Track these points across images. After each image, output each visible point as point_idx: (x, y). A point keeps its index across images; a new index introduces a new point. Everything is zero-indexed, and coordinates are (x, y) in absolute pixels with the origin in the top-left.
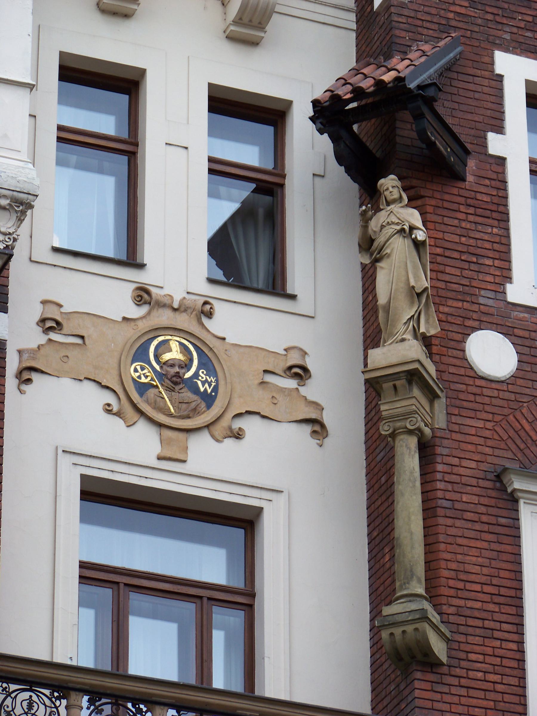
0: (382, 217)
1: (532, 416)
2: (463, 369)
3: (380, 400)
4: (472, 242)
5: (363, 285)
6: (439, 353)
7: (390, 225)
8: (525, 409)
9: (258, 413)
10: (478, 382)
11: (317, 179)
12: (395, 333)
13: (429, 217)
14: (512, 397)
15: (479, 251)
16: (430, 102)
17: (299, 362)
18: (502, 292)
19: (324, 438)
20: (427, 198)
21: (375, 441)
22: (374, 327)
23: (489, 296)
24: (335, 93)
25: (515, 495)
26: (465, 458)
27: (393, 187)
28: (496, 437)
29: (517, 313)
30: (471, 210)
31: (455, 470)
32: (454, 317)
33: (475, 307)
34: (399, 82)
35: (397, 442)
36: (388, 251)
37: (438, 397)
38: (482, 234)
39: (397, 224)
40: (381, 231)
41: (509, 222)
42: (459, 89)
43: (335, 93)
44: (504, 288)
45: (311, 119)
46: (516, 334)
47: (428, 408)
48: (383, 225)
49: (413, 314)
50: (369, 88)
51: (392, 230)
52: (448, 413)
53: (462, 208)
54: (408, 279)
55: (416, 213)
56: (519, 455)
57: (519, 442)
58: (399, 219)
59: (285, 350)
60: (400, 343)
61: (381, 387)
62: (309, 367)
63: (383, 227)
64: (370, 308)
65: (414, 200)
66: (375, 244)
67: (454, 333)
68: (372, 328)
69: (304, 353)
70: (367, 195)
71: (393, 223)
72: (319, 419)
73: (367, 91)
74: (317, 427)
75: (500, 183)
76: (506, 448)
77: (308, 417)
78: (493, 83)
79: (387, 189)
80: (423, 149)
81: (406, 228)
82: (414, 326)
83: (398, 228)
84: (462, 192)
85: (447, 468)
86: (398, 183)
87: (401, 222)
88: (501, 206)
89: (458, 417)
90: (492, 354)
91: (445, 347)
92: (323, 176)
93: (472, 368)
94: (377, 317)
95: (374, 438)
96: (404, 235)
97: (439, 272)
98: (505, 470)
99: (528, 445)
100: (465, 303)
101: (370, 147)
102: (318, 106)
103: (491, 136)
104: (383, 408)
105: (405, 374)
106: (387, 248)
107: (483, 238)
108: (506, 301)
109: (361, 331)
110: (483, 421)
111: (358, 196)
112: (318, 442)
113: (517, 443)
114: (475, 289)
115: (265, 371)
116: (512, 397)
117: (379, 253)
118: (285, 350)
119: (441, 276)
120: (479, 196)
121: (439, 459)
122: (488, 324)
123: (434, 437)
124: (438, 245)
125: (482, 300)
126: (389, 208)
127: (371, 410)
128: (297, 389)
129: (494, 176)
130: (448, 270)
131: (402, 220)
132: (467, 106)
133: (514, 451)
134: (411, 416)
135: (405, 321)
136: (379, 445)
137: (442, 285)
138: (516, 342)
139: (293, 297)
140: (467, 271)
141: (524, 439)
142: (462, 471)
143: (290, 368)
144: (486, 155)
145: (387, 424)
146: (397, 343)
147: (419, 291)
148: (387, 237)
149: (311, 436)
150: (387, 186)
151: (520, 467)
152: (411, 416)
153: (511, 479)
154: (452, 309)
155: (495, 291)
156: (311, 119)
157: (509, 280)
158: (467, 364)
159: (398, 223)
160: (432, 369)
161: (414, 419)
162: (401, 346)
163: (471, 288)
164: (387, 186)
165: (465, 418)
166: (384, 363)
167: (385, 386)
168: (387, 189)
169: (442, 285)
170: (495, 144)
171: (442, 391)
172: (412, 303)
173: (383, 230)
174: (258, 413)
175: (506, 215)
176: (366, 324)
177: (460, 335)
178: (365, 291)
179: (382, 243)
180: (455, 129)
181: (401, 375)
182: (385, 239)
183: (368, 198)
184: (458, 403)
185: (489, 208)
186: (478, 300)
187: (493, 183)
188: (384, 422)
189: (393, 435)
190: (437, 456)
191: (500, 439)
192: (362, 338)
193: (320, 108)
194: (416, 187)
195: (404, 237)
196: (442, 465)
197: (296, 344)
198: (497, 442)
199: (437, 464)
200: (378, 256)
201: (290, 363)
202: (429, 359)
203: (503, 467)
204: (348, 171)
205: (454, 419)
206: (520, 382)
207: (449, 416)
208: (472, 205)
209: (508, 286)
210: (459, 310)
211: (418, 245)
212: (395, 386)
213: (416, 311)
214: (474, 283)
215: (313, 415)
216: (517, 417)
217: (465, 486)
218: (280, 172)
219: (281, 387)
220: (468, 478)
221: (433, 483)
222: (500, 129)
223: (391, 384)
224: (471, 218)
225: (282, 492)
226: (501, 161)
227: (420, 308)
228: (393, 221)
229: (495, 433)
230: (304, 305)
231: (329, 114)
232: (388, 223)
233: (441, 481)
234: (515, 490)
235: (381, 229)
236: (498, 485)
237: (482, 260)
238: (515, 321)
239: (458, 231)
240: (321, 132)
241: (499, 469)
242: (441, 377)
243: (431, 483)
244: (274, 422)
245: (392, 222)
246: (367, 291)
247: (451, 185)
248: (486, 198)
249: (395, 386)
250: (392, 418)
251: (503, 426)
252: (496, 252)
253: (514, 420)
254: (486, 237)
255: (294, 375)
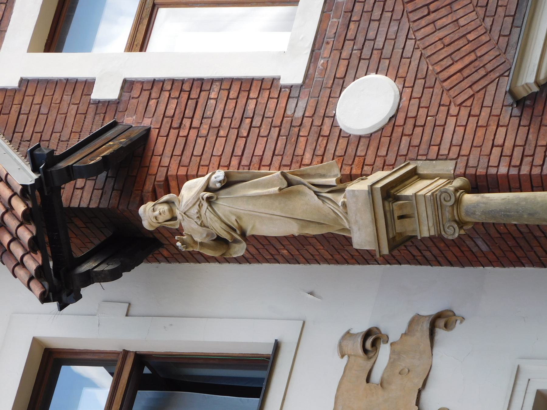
0: (190, 227)
1: (445, 60)
2: (382, 139)
3: (417, 236)
4: (226, 123)
5: (267, 261)
6: (361, 167)
7: (201, 215)
8: (436, 68)
9: (420, 392)
10: (400, 120)
11: (132, 311)
12: (334, 215)
13: (192, 171)
14: (420, 82)
15: (238, 115)
16: (52, 159)
17: (359, 340)
18: (290, 90)
19: (454, 315)
20: (169, 173)
21: (463, 252)
22: (322, 248)
23: (294, 105)
24: (34, 275)
25: (543, 83)
26: (493, 140)
27: (154, 210)
28: (468, 103)
29: (316, 73)
30: (187, 122)
31: (507, 152)
32: (318, 147)
33: (307, 122)
34: (28, 193)
35: (468, 219)
36: (233, 218)
37: (415, 169)
38: (217, 111)
39: (200, 206)
40: (208, 228)
41: (203, 79)
42: (35, 131)
43: (34, 275)
44: (286, 87)
45: (61, 307)
46: (343, 76)
47: (428, 182)
48: (201, 224)
49: (312, 192)
50: (31, 232)
51: (208, 213)
52: (437, 159)
53: (183, 133)
54: (269, 196)
55: (187, 184)
56: (493, 76)
57: (476, 76)
58: (194, 204)
59: (342, 356)
60: (348, 208)
61: (400, 234)
62: (364, 328)
63: (202, 225)
64: (297, 253)
65: (171, 185)
66: (224, 235)
67: (338, 148)
68: (323, 252)
69: (348, 334)
70: (157, 252)
71: (199, 212)
72: (430, 319)
73: (35, 233)
74: (442, 321)
75: (154, 87)
76: (483, 92)
77: (427, 333)
78: (30, 91)
79: (156, 218)
80: (107, 177)
81: (208, 194)
82: (328, 192)
83: (205, 204)
84: (164, 132)
85: (505, 161)
86: (150, 204)
87: (198, 201)
88: (183, 87)
89: (442, 147)
90: (368, 103)
91: (354, 159)
92: (130, 304)
93: (382, 129)
94: (314, 237)
95: (459, 254)
96: (215, 199)
97: (260, 163)
98: (511, 92)
99: (481, 65)
100: (301, 134)
101: (102, 240)
102: (48, 296)
103: (97, 95)
104: (426, 234)
105: (386, 203)
106: (230, 221)
107: (222, 109)
108: (302, 86)
109: (324, 267)
110: (448, 117)
111: (155, 265)
112: (458, 322)
113: (478, 78)
114: (284, 121)
115: (368, 380)
116: (420, 82)
117: (234, 230)
118: (342, 356)
119: (267, 160)
120: (170, 112)
121: (493, 171)
122: (328, 107)
123: (464, 175)
124: (228, 163)
125: (299, 114)
126: (179, 217)
127: (424, 256)
128: (391, 344)
129: (146, 94)
130: (259, 152)
131: (196, 200)
132: (56, 122)
133: (487, 83)
134: (438, 199)
135: (320, 202)
136: (469, 247)
137: (277, 160)
138: (353, 76)
139: (277, 346)
140: (262, 131)
141: (474, 70)
142: (509, 144)
143: (365, 351)
144: (118, 103)
145: (447, 229)
146: (347, 213)
147: (285, 184)
148: (216, 219)
149: (452, 329)
150: (152, 219)
151: (508, 76)
152: (438, 199)
153: (523, 86)
154: (308, 149)
155: (289, 97)
156: (61, 307)
157: (275, 81)
158: (376, 134)
159: (199, 205)
160: (380, 174)
161: (443, 195)
162: (351, 208)
163: (283, 125)
164: (152, 219)
165: (443, 138)
166: (371, 229)
167: (399, 229)
168: (156, 218)
169: (277, 160)
170: (107, 90)
171: (408, 164)
172: (299, 192)
173: (206, 225)
174: (420, 392)
175: (195, 83)
176: (316, 260)
177: (340, 141)
178: (275, 259)
179: (224, 226)
180: (85, 136)
181: (387, 208)
182: (219, 221)
183: (161, 250)
184: (424, 147)
185: (186, 101)
186: (298, 118)
187: (154, 95)
188: (443, 233)
189: (461, 224)
190: (488, 173)
191: (472, 99)
192: (332, 266)
193: (51, 294)
194: (154, 185)
195: (217, 199)
196: (500, 167)
197: (337, 342)
198: (475, 102)
199: (498, 173)
200: (238, 232)
201: (360, 352)
202: (369, 177)
203: (508, 94)
204: (129, 268)
205: (444, 151)
206: (402, 72)
207: (439, 157)
208: (180, 121)
209: (283, 81)
210: (309, 141)
211: (228, 183)
212: (401, 217)
213: (309, 188)
214: (277, 122)
215: (426, 326)
216: (446, 77)
217: (528, 142)
218: (121, 356)
219: (388, 364)
220: (518, 138)
221: (522, 179)
222: (88, 85)
223: (398, 222)
224: (196, 123)
225: (519, 367)
226: (128, 85)
227: (307, 183)
228: (197, 211)
229: (464, 104)
230: (288, 334)
231: (60, 286)
232: (198, 217)
233: (519, 170)
234: (536, 82)
235: (205, 226)
236: (528, 102)
237: (249, 112)
238: (326, 76)
239: (211, 138)
240: (79, 297)
241: (510, 100)
242: (390, 165)
243: (522, 182)
244: (431, 373)
245: (197, 213)
246: (276, 257)
247: (152, 148)
248: (173, 104)
249: (401, 217)
250: (438, 223)
251: (456, 94)
252: (240, 95)
253: (449, 81)
254: (221, 106)
255: (374, 348)
